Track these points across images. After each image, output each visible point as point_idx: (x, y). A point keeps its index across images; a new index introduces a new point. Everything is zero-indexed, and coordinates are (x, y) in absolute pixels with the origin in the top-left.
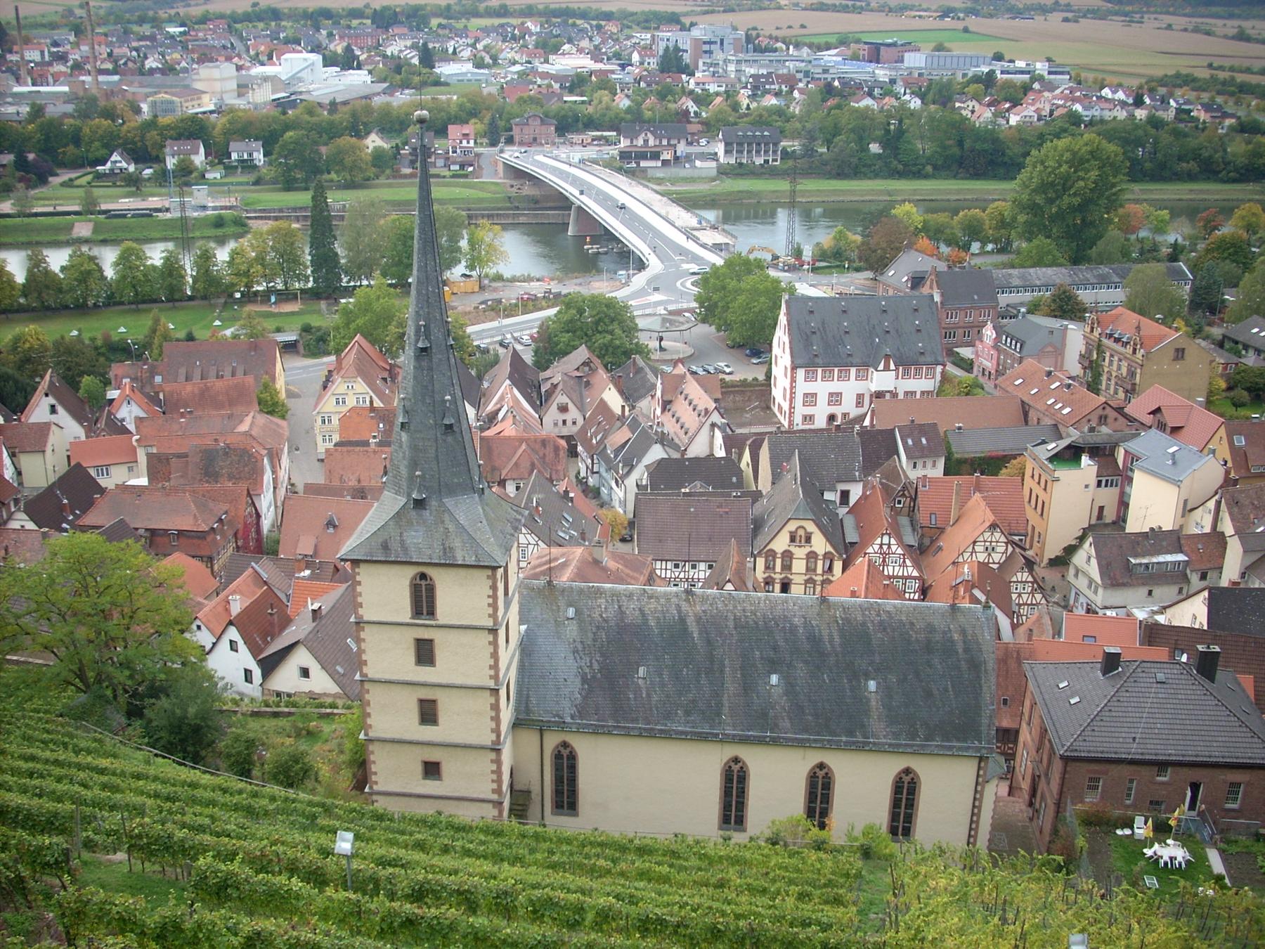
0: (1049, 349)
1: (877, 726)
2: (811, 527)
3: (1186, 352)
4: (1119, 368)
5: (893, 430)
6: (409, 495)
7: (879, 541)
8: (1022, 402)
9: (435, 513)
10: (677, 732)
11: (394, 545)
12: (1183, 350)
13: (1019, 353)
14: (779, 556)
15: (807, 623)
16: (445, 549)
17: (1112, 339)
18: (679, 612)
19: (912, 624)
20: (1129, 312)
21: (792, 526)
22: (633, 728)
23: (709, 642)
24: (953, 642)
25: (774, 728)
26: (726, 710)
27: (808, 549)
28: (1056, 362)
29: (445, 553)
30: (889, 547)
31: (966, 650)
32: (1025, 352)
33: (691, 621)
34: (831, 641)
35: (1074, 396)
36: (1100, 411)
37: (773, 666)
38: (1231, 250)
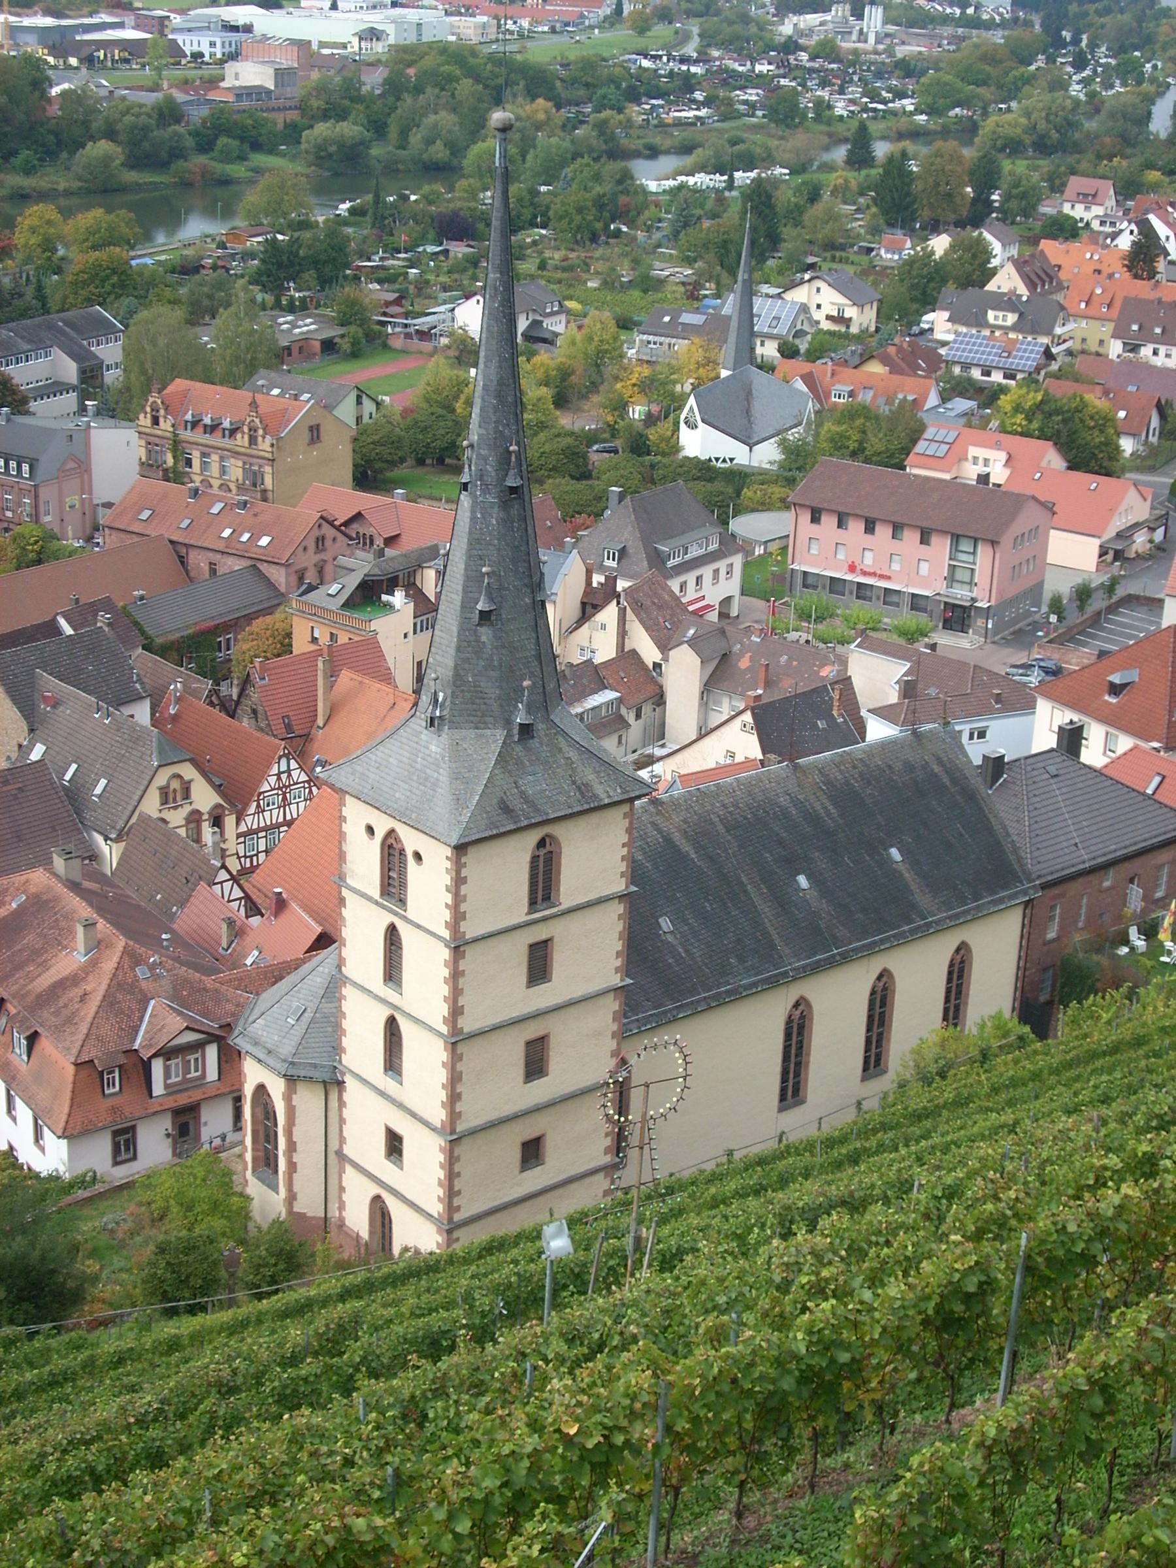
0: (72, 465)
1: (923, 899)
2: (188, 771)
3: (322, 429)
4: (223, 471)
5: (54, 622)
6: (508, 723)
7: (275, 770)
8: (172, 542)
9: (545, 739)
10: (746, 987)
11: (516, 804)
12: (318, 426)
13: (30, 479)
14: (206, 817)
15: (796, 803)
16: (579, 788)
17: (200, 429)
18: (660, 831)
19: (890, 767)
20: (199, 384)
21: (162, 779)
22: (698, 1001)
23: (711, 859)
24: (936, 775)
25: (837, 942)
26: (777, 940)
27: (187, 809)
28: (82, 483)
29: (582, 793)
30: (290, 775)
31: (954, 781)
32: (40, 477)
33: (677, 837)
34: (829, 814)
35: (260, 519)
36: (316, 533)
37: (793, 865)
38: (115, 279)
